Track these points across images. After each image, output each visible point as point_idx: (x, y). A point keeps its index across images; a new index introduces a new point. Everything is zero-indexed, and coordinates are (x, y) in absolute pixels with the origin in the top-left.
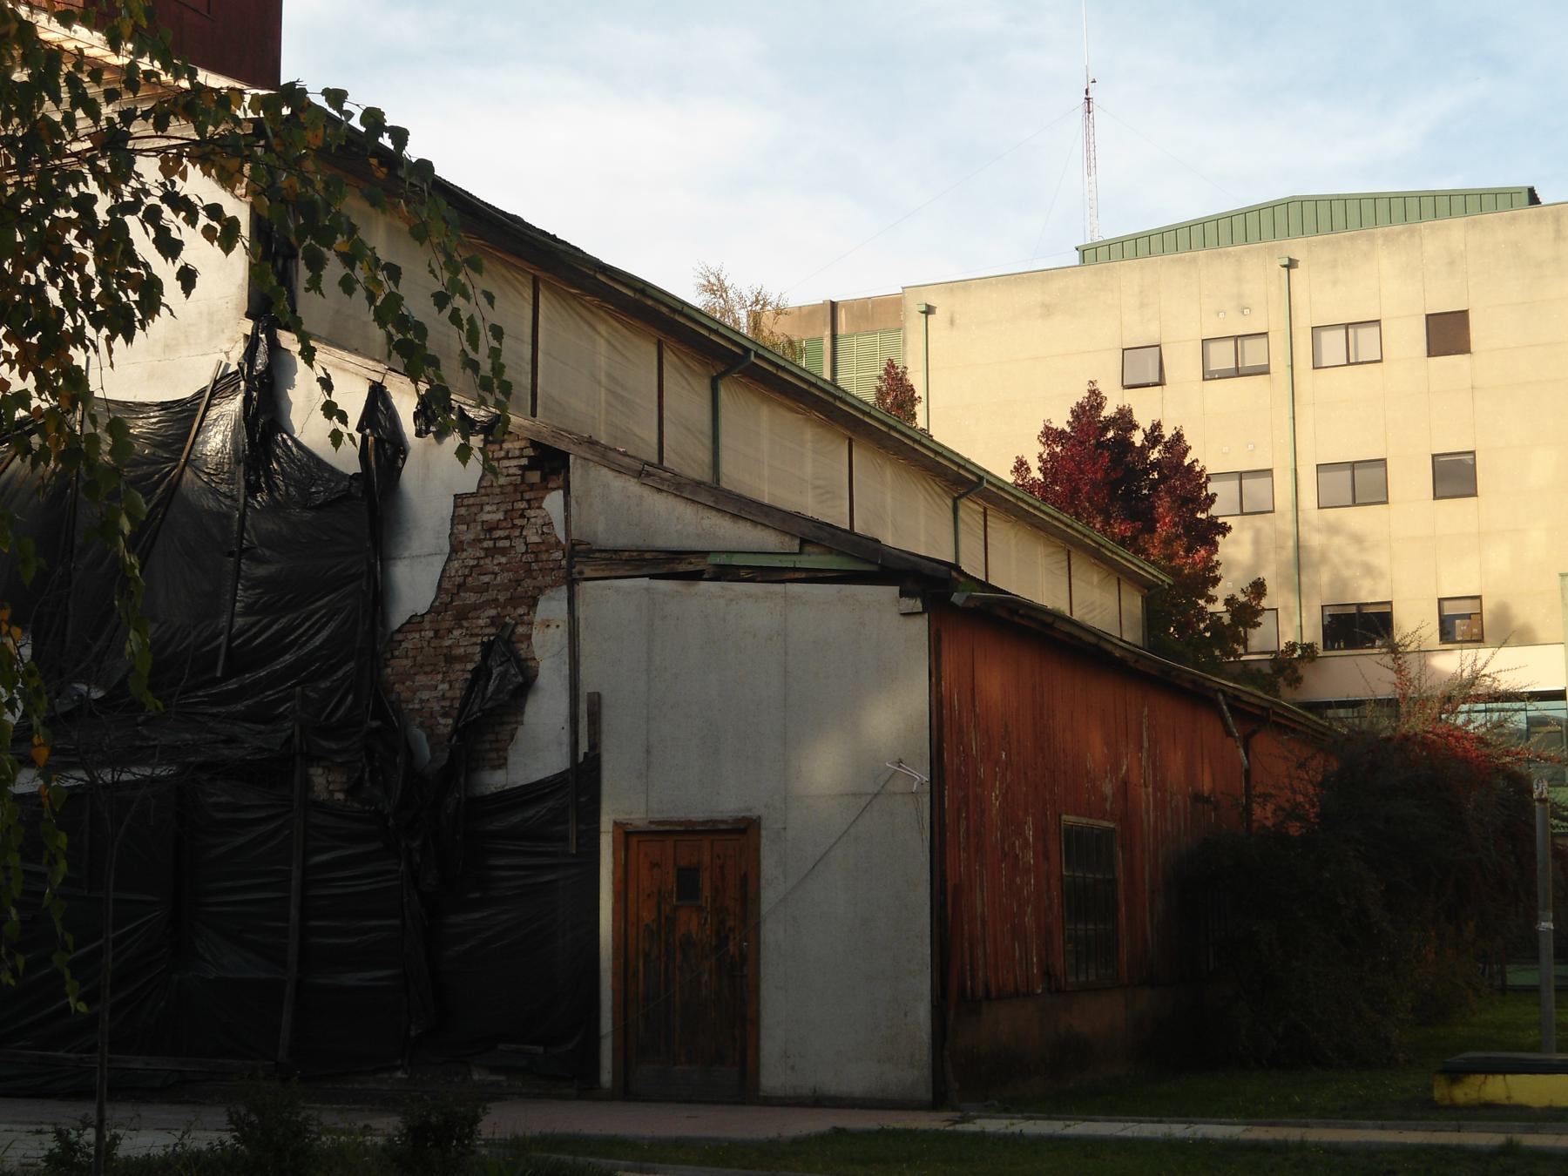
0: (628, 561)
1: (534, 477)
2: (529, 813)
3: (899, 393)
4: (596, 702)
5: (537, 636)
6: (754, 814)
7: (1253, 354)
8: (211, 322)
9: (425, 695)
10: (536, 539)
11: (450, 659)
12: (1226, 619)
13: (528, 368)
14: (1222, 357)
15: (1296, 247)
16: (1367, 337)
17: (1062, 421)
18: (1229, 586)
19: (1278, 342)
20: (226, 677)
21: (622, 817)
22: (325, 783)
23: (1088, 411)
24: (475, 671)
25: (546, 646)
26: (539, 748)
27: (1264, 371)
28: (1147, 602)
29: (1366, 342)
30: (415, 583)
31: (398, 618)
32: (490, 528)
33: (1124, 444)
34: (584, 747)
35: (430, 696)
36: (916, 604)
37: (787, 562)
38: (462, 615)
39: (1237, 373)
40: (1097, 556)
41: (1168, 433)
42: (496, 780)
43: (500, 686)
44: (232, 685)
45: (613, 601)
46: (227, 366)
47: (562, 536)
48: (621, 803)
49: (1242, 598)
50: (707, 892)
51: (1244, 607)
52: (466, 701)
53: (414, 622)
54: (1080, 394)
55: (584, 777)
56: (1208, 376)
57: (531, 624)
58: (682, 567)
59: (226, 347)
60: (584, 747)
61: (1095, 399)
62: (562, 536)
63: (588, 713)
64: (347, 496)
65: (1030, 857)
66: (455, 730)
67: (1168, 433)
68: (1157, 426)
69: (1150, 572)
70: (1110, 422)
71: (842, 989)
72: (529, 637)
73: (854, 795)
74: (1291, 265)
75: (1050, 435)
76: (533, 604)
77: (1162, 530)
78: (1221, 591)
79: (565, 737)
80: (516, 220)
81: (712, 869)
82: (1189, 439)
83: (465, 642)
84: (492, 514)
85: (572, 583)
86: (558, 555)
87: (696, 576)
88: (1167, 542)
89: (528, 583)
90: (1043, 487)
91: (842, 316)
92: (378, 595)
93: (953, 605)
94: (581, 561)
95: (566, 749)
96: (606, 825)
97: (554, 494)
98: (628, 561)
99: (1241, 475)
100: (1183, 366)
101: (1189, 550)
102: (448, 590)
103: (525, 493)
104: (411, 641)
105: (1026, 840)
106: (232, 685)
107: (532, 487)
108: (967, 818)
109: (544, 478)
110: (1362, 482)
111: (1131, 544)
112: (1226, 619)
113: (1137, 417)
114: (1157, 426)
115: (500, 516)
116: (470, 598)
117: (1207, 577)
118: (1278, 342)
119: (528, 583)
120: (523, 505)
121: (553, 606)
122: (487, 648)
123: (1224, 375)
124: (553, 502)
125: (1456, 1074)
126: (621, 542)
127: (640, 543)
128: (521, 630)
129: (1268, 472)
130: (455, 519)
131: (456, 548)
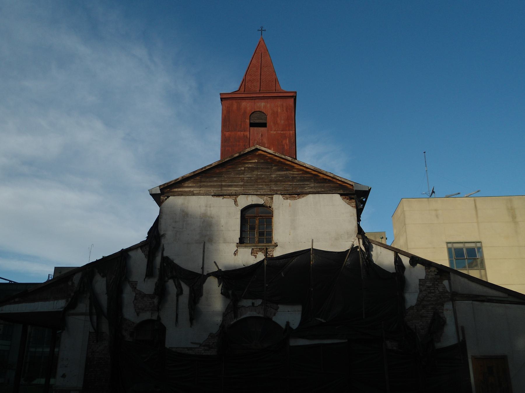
4: (463, 328)
5: (445, 312)
8: (348, 234)
10: (441, 290)
26: (449, 337)
30: (411, 298)
32: (429, 287)
34: (461, 338)
42: (438, 345)
43: (438, 323)
45: (463, 305)
46: (353, 245)
47: (449, 290)
48: (472, 352)
53: (412, 308)
57: (443, 310)
59: (353, 241)
62: (449, 290)
63: (461, 330)
72: (443, 312)
73: (514, 217)
76: (443, 305)
84: (428, 284)
86: (447, 294)
87: (483, 301)
92: (403, 300)
93: (290, 302)
96: (469, 356)
97: (373, 253)
102: (420, 301)
115: (431, 285)
120: (437, 283)
121: (448, 306)
130: (420, 285)
131: (421, 291)
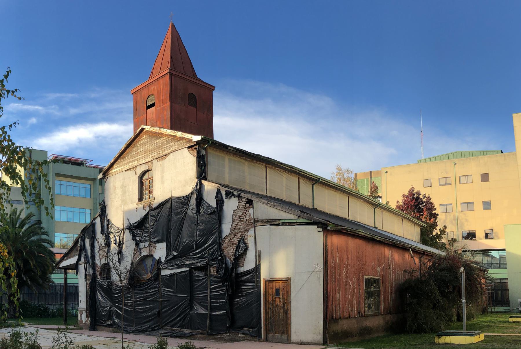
0: (265, 222)
1: (248, 205)
2: (247, 277)
3: (375, 190)
6: (289, 277)
7: (448, 181)
9: (229, 252)
11: (233, 244)
12: (439, 233)
13: (265, 184)
14: (443, 182)
15: (456, 161)
16: (469, 178)
17: (406, 193)
18: (440, 226)
19: (453, 178)
20: (196, 250)
21: (265, 278)
22: (213, 271)
23: (411, 191)
24: (237, 246)
25: (250, 241)
27: (450, 184)
28: (422, 230)
29: (469, 179)
31: (224, 236)
33: (418, 198)
35: (229, 251)
36: (320, 229)
37: (295, 221)
38: (235, 235)
39: (446, 184)
40: (409, 219)
41: (427, 196)
42: (242, 270)
44: (198, 251)
45: (263, 230)
49: (442, 229)
50: (281, 294)
51: (442, 231)
52: (235, 253)
54: (410, 188)
55: (257, 269)
56: (440, 185)
58: (276, 223)
60: (258, 262)
61: (413, 189)
64: (214, 211)
65: (355, 285)
66: (234, 259)
67: (427, 196)
68: (425, 194)
69: (421, 223)
70: (416, 193)
71: (306, 318)
74: (455, 164)
75: (404, 196)
77: (425, 215)
78: (438, 228)
79: (254, 260)
80: (269, 158)
81: (282, 291)
82: (431, 197)
83: (235, 240)
85: (255, 227)
87: (278, 225)
88: (426, 218)
89: (247, 227)
90: (402, 206)
91: (372, 174)
94: (256, 222)
95: (254, 263)
98: (265, 222)
99: (446, 205)
100: (435, 183)
101: (430, 219)
102: (233, 230)
103: (246, 209)
104: (226, 241)
105: (354, 282)
106: (198, 251)
107: (247, 207)
108: (335, 277)
109: (250, 206)
110: (469, 205)
111: (418, 218)
112: (439, 233)
113: (421, 193)
114: (425, 194)
116: (237, 231)
117: (435, 225)
118: (453, 178)
119: (247, 227)
121: (251, 232)
122: (239, 241)
123: (443, 185)
124: (251, 210)
125: (440, 336)
126: (264, 218)
127: (268, 218)
128: (246, 237)
129: (451, 204)
